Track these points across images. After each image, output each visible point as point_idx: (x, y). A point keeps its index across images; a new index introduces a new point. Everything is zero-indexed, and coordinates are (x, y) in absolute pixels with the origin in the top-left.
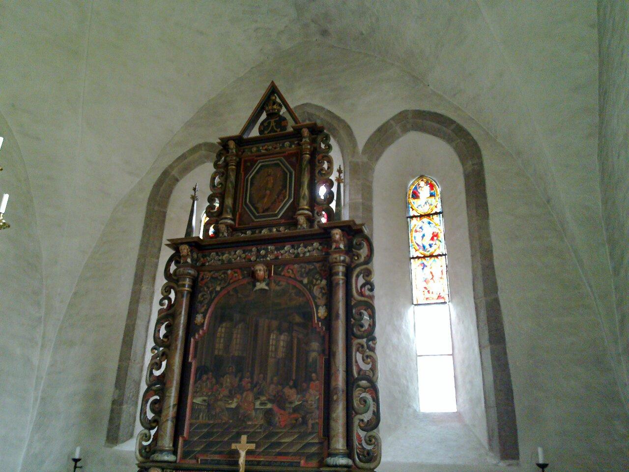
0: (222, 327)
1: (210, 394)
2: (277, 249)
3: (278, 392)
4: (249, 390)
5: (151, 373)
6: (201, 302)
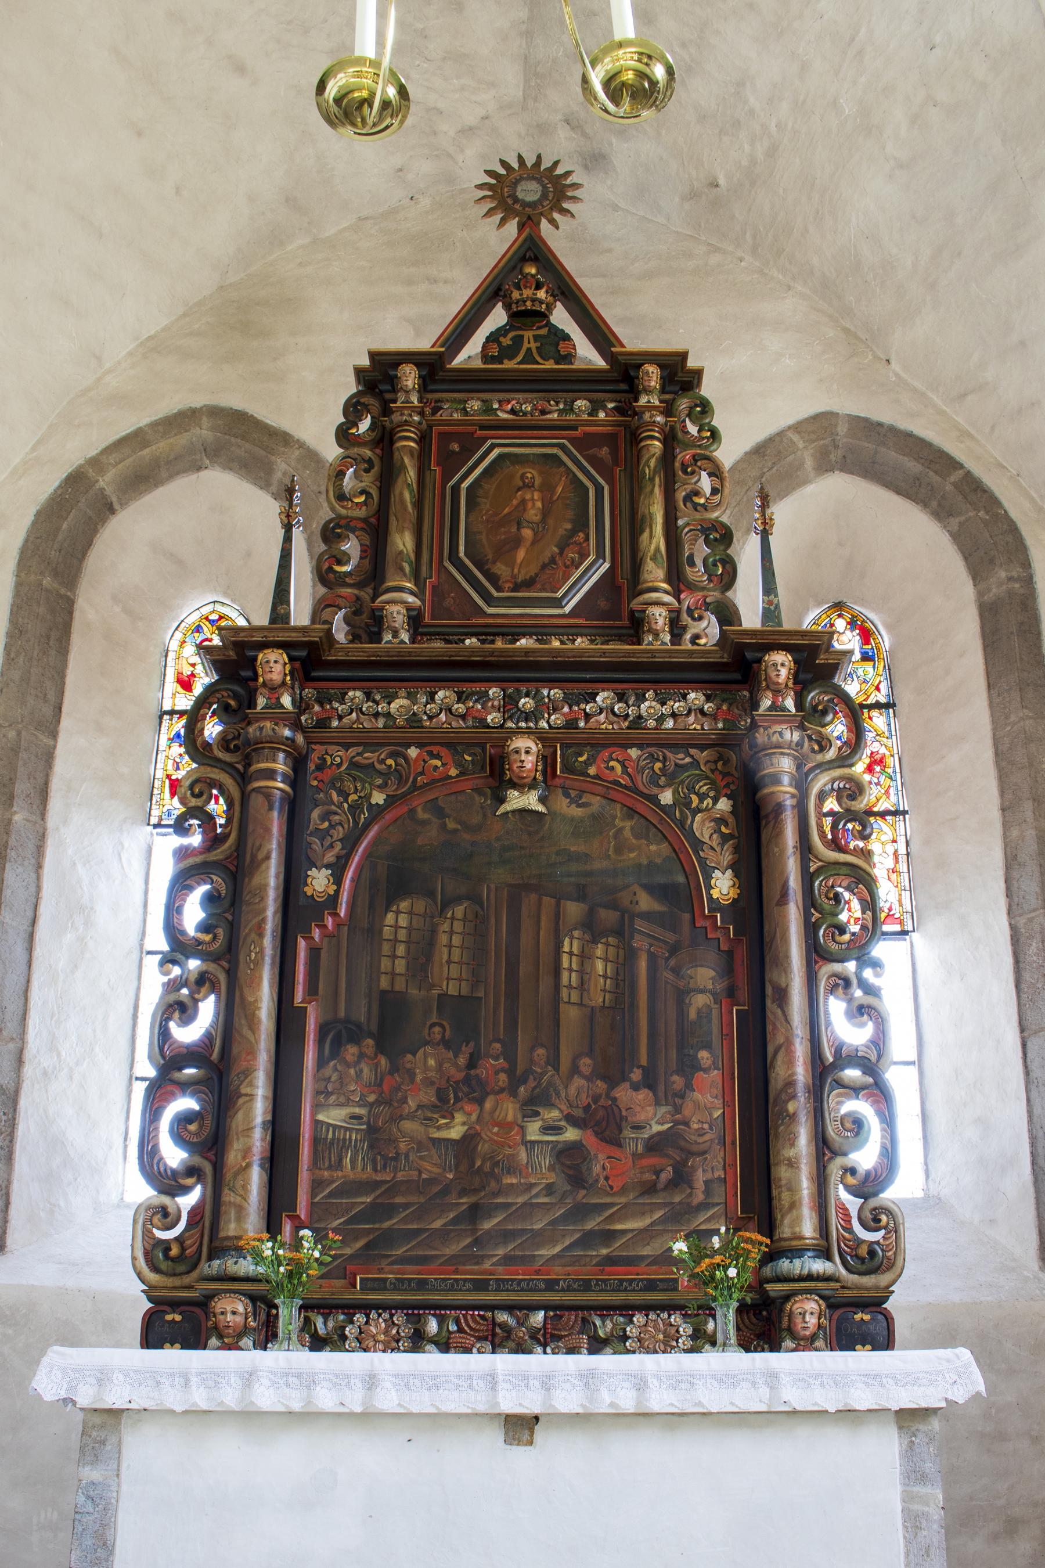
0: (398, 912)
1: (372, 1098)
2: (570, 700)
3: (596, 1099)
4: (502, 1090)
5: (163, 1035)
6: (323, 835)
